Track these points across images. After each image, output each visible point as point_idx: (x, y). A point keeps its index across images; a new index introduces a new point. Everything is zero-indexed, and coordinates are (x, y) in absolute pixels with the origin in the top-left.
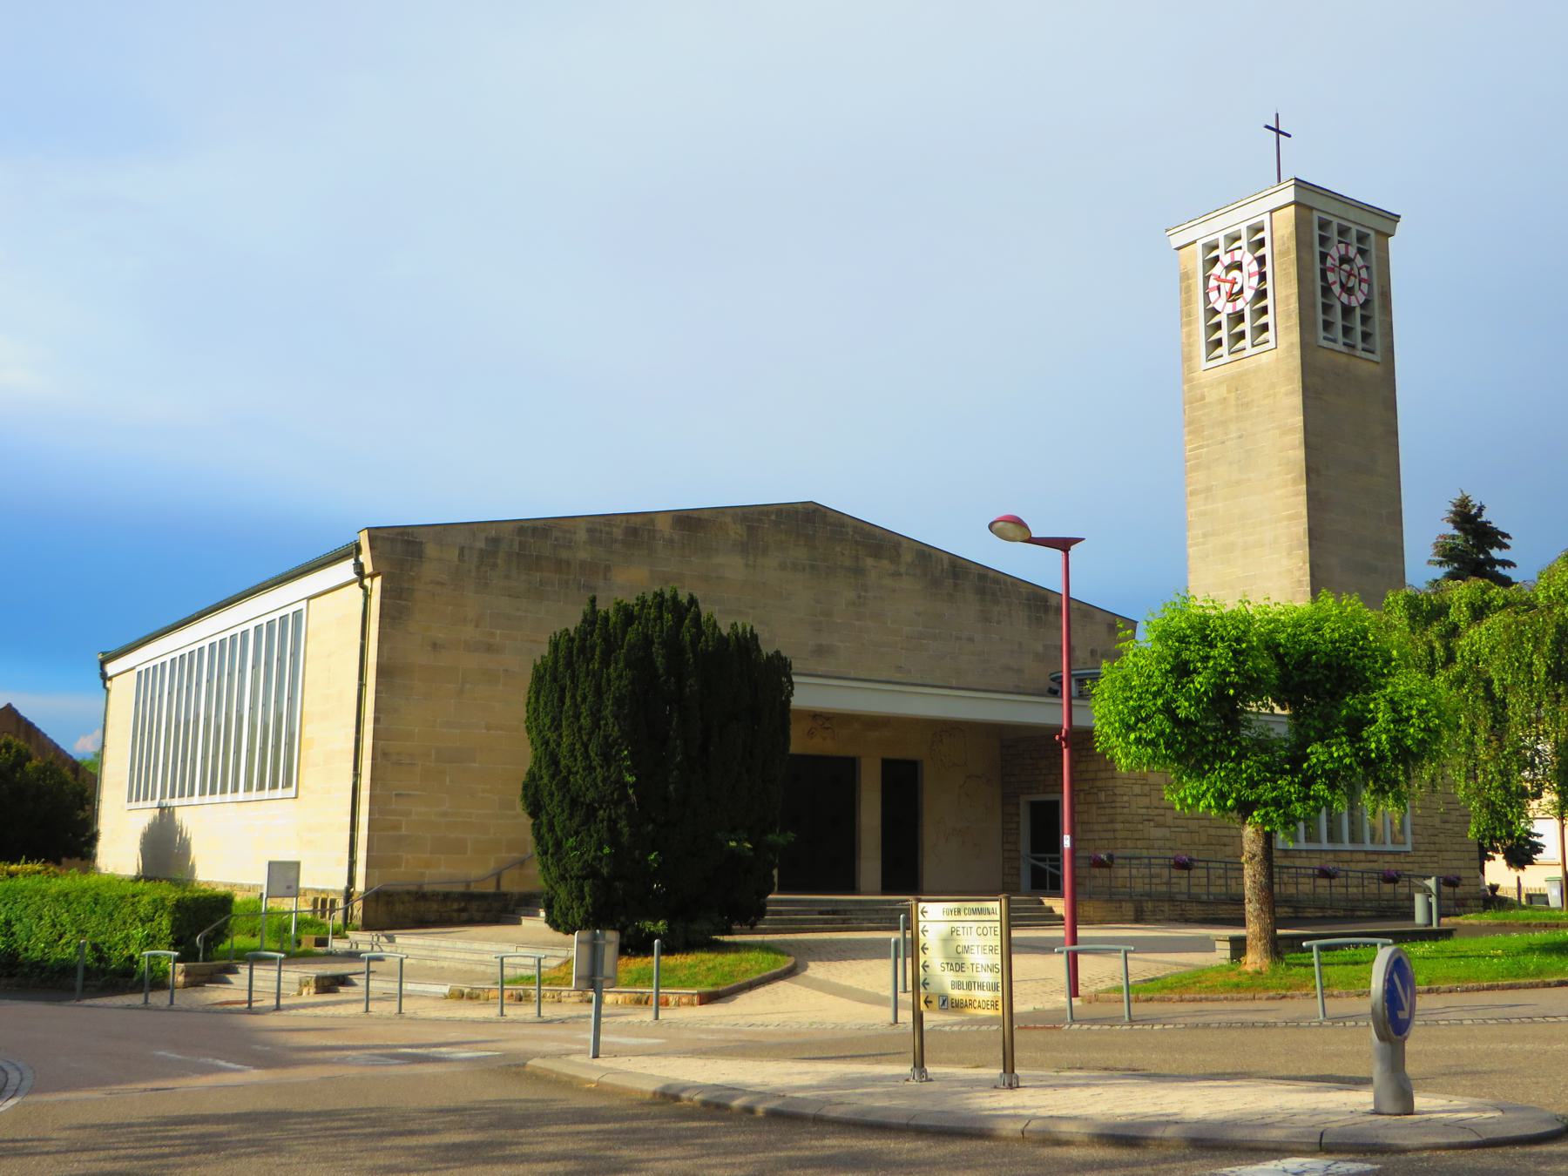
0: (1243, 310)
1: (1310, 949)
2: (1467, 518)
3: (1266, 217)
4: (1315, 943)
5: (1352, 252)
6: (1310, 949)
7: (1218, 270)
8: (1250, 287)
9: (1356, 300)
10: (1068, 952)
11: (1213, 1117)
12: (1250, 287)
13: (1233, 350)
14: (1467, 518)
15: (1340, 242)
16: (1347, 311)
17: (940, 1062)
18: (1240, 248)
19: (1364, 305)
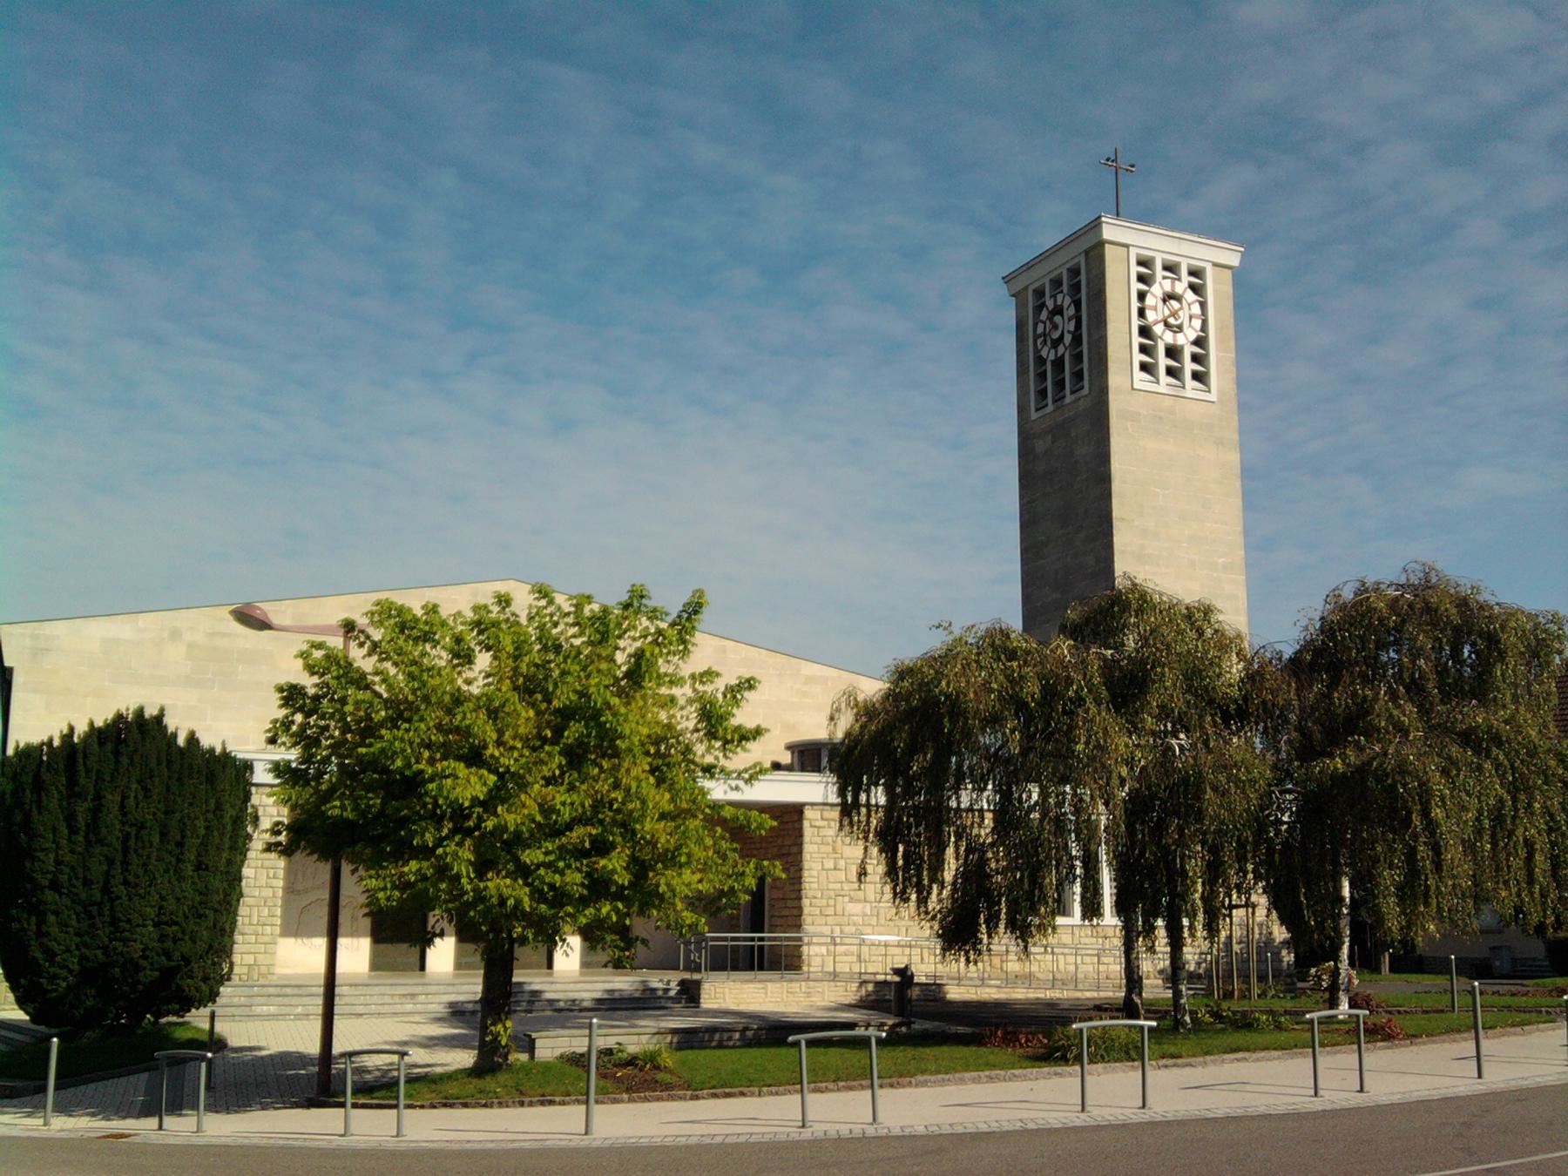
0: (1063, 355)
1: (797, 1044)
2: (353, 874)
3: (1082, 260)
4: (802, 1038)
5: (1180, 287)
6: (797, 1044)
7: (1044, 315)
8: (1069, 332)
9: (1185, 340)
10: (1368, 1042)
11: (348, 972)
12: (1069, 332)
13: (1074, 389)
14: (353, 874)
15: (1164, 278)
16: (1172, 352)
17: (519, 975)
18: (1062, 292)
19: (1200, 342)
